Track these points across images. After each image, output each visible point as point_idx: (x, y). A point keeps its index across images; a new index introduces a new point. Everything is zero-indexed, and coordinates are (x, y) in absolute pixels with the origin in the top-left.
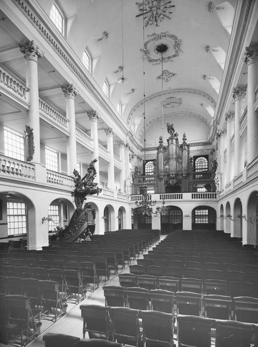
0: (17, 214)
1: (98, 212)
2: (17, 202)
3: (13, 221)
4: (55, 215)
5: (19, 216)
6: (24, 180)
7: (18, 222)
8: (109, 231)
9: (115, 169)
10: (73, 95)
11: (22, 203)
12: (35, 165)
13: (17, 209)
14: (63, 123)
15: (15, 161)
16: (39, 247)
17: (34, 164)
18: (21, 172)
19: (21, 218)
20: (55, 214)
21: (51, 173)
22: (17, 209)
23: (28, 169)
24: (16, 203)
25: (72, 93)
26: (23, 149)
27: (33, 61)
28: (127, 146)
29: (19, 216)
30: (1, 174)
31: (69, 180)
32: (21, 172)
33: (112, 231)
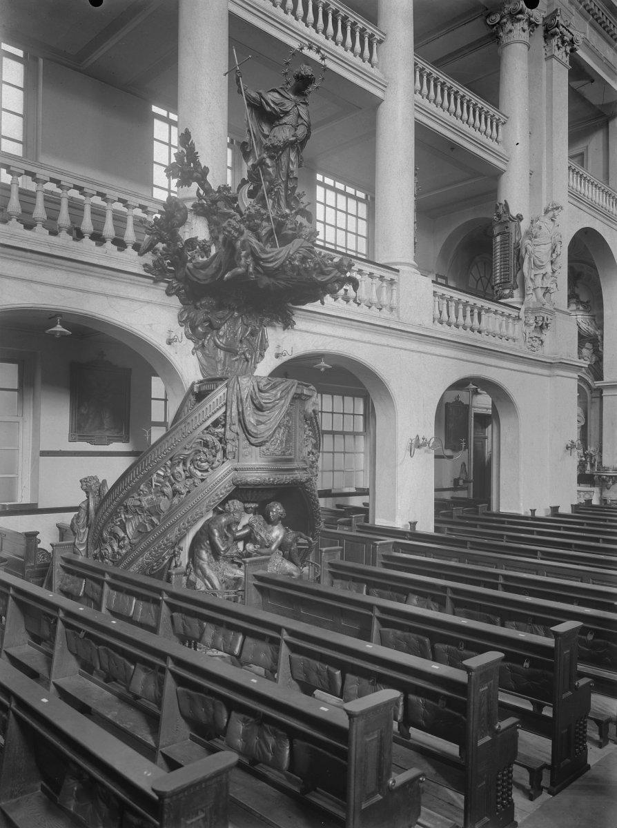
0: (330, 429)
1: (517, 417)
2: (344, 394)
3: (332, 450)
4: (351, 430)
5: (346, 436)
6: (497, 345)
7: (333, 453)
8: (494, 510)
9: (233, 41)
10: (524, 31)
11: (358, 396)
12: (398, 271)
13: (343, 414)
14: (483, 127)
15: (364, 265)
16: (243, 574)
17: (396, 267)
18: (465, 320)
19: (343, 440)
20: (348, 429)
21: (383, 274)
22: (343, 414)
23: (377, 281)
24: (351, 398)
25: (522, 22)
26: (156, 144)
27: (514, 44)
28: (548, 34)
29: (346, 436)
30: (2, 255)
31: (509, 316)
32: (465, 320)
33: (502, 510)
